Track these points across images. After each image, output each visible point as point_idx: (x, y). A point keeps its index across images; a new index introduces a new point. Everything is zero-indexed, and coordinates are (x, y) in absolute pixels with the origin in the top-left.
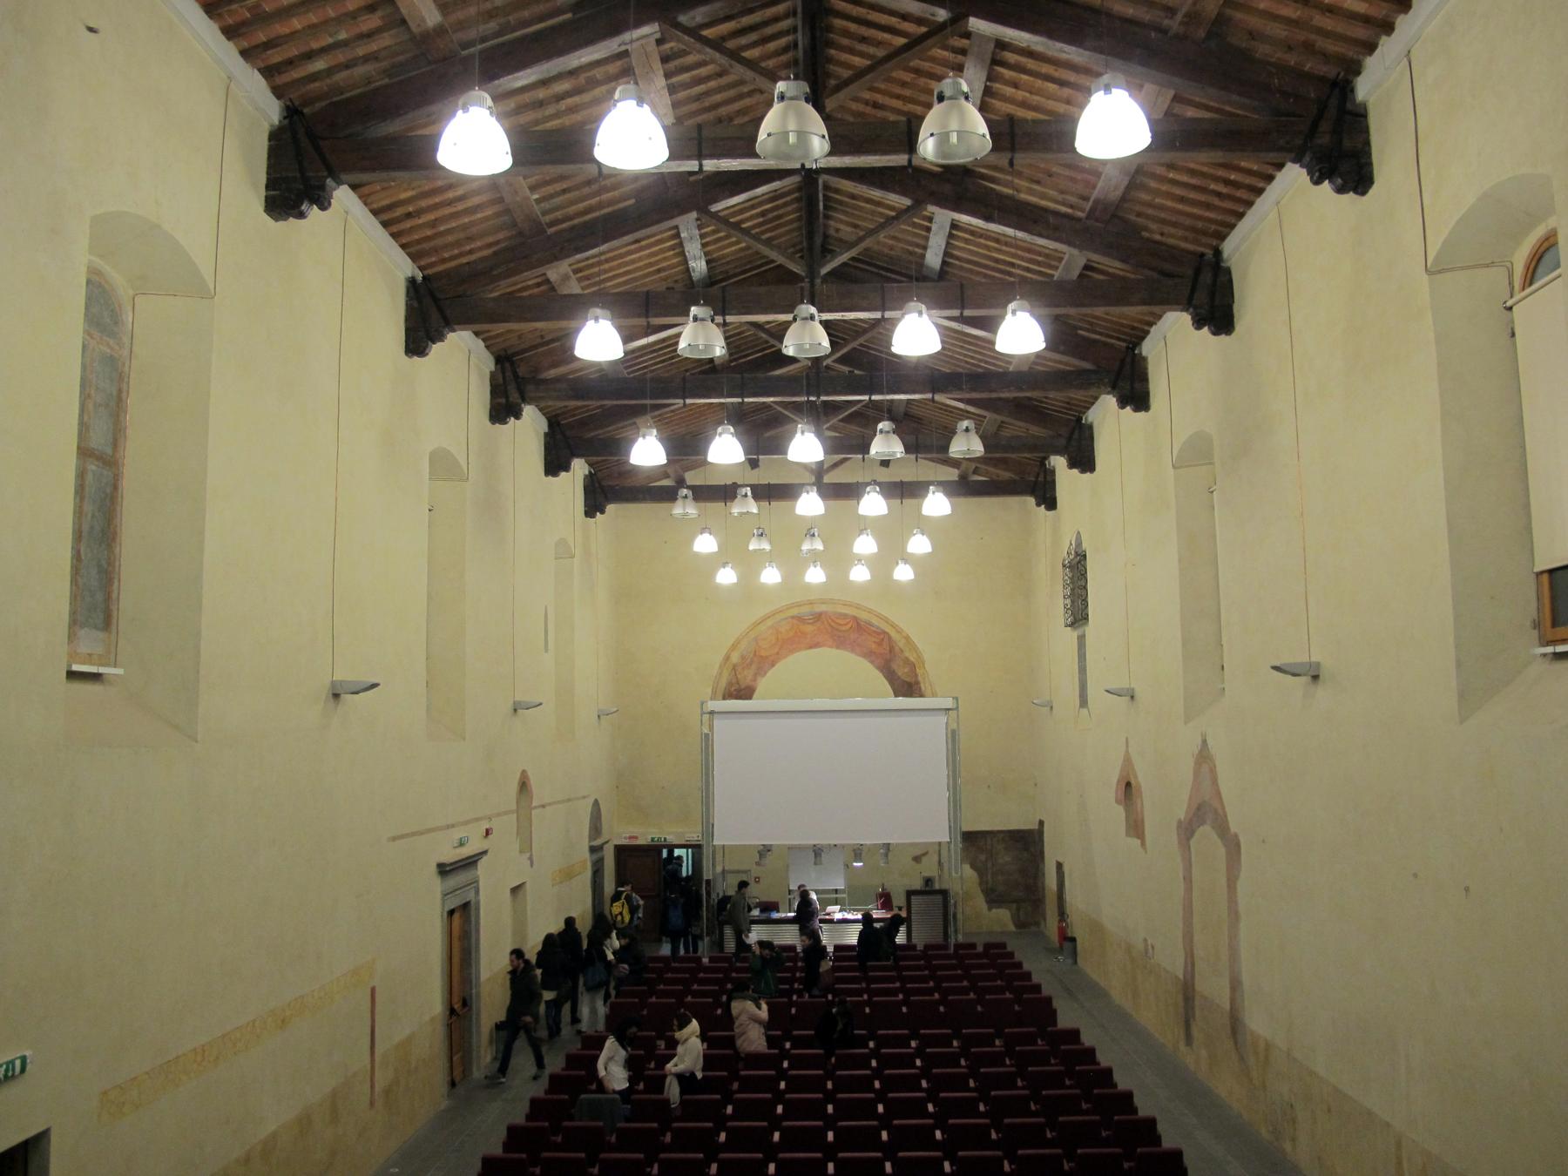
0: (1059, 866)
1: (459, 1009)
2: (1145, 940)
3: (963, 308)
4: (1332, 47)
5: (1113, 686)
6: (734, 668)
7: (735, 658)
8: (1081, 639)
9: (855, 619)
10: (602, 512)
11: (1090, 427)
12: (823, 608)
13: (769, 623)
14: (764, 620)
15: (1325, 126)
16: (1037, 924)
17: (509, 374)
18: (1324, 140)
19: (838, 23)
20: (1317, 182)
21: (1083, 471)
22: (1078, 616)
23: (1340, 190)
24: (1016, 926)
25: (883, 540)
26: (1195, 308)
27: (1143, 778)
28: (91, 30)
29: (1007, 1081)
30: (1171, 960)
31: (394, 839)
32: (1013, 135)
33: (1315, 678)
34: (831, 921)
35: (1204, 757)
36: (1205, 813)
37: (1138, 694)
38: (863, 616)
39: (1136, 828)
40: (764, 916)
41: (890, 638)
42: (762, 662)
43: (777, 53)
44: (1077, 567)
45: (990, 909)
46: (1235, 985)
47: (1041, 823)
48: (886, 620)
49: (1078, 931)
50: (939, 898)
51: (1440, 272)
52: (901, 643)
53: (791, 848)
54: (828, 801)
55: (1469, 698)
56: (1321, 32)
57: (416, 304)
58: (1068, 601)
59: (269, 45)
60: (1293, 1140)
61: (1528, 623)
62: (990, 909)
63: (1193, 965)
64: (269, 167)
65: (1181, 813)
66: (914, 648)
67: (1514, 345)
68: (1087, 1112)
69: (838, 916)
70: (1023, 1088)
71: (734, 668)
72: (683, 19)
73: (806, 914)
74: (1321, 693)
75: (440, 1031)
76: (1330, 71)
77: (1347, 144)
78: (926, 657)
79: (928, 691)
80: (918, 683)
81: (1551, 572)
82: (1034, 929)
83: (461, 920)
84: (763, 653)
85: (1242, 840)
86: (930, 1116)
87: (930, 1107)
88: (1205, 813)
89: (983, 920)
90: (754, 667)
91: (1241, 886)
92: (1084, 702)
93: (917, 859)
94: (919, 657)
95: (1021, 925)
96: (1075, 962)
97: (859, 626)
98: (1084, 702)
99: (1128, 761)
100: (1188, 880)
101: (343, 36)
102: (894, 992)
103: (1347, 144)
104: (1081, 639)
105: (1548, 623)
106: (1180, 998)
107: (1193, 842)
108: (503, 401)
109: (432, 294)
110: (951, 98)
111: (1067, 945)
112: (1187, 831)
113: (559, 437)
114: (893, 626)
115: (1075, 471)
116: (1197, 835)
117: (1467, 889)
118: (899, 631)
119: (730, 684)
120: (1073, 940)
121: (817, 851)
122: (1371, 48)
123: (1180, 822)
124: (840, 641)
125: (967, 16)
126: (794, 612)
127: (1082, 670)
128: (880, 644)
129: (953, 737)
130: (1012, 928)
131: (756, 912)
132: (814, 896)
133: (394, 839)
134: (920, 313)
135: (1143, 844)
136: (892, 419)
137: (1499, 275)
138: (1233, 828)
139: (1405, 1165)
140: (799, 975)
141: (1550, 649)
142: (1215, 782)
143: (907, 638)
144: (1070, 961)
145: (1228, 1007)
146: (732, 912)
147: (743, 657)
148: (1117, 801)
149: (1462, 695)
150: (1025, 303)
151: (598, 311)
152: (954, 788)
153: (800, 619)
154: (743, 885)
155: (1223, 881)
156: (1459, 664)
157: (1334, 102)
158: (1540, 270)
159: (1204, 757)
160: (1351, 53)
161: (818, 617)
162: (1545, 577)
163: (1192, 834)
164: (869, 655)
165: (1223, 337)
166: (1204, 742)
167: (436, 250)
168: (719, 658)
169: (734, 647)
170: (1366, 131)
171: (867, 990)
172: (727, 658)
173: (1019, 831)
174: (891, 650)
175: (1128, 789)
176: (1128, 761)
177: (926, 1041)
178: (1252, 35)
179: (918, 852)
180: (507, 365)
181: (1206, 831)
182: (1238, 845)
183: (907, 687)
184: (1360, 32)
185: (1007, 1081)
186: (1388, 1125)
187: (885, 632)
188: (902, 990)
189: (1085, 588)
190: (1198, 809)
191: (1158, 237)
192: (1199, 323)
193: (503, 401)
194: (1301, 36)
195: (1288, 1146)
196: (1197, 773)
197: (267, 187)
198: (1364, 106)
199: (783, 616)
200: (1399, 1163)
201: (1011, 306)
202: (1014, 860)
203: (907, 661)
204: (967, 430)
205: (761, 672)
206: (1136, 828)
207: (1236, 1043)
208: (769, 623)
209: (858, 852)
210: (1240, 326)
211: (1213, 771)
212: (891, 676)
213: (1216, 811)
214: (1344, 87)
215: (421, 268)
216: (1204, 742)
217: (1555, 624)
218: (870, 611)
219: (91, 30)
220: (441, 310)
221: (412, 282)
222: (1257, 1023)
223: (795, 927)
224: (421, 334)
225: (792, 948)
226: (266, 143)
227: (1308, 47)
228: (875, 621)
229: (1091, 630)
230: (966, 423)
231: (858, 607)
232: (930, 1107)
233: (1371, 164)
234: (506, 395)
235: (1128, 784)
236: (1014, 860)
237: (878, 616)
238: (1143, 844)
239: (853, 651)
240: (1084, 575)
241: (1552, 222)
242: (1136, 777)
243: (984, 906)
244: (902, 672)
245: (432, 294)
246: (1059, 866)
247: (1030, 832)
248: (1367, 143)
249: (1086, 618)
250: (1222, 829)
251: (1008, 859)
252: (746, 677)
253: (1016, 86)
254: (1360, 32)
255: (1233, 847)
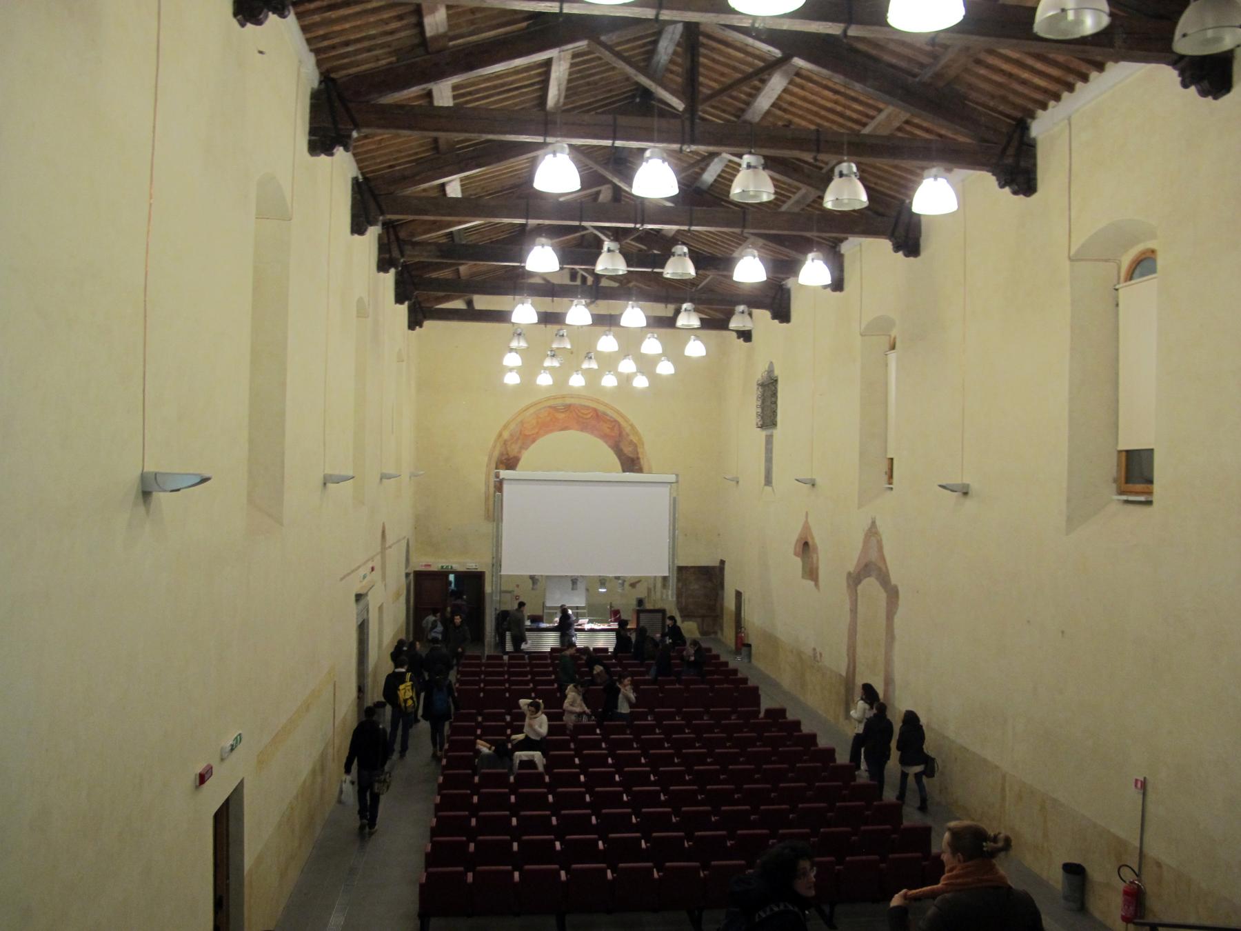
0: (739, 595)
3: (744, 227)
6: (505, 443)
7: (506, 435)
9: (595, 410)
11: (788, 291)
13: (532, 410)
14: (527, 409)
15: (1011, 151)
16: (716, 633)
17: (393, 237)
18: (1009, 161)
19: (702, 50)
21: (782, 322)
22: (768, 418)
23: (1015, 193)
25: (633, 355)
27: (819, 539)
28: (261, 52)
30: (837, 662)
31: (342, 579)
32: (818, 140)
33: (966, 494)
34: (583, 630)
35: (872, 532)
36: (870, 568)
37: (819, 481)
38: (601, 408)
39: (811, 573)
40: (535, 626)
41: (620, 425)
42: (526, 439)
44: (769, 388)
47: (722, 562)
49: (752, 640)
50: (659, 615)
52: (628, 429)
53: (547, 577)
54: (581, 544)
56: (1015, 92)
63: (854, 667)
65: (851, 567)
69: (587, 627)
70: (668, 748)
71: (505, 443)
73: (565, 626)
74: (969, 503)
75: (355, 703)
76: (1019, 115)
77: (1022, 164)
79: (645, 467)
81: (1127, 451)
84: (527, 433)
85: (900, 589)
88: (870, 568)
91: (898, 620)
92: (768, 481)
93: (633, 585)
97: (598, 416)
98: (768, 481)
100: (854, 611)
102: (527, 683)
105: (1123, 479)
106: (843, 691)
107: (860, 587)
108: (387, 256)
109: (371, 191)
111: (744, 650)
112: (855, 580)
118: (627, 421)
119: (502, 454)
120: (749, 646)
121: (574, 581)
122: (1044, 107)
124: (584, 426)
126: (551, 403)
127: (769, 460)
128: (612, 429)
129: (674, 503)
131: (528, 623)
132: (570, 612)
133: (342, 579)
135: (817, 585)
138: (894, 580)
141: (1125, 498)
142: (880, 548)
143: (632, 426)
144: (746, 660)
146: (513, 623)
148: (796, 554)
149: (1069, 519)
151: (543, 240)
152: (673, 538)
153: (555, 408)
154: (522, 604)
156: (1069, 501)
158: (1137, 272)
159: (872, 532)
160: (1030, 106)
161: (568, 408)
163: (859, 582)
164: (604, 437)
166: (874, 523)
167: (373, 158)
168: (494, 436)
169: (505, 427)
170: (1034, 157)
171: (508, 681)
172: (500, 435)
174: (620, 434)
175: (805, 547)
177: (659, 718)
183: (631, 463)
187: (616, 421)
188: (532, 681)
189: (775, 403)
190: (866, 565)
192: (897, 248)
193: (387, 256)
198: (1034, 140)
201: (810, 256)
203: (631, 442)
205: (525, 446)
206: (811, 573)
208: (532, 410)
209: (603, 581)
210: (925, 254)
211: (880, 543)
213: (880, 569)
216: (874, 523)
217: (1127, 481)
218: (606, 405)
219: (261, 52)
221: (355, 180)
223: (557, 634)
225: (606, 650)
227: (1004, 99)
228: (609, 412)
229: (777, 433)
231: (597, 401)
234: (390, 251)
235: (806, 544)
237: (612, 408)
238: (817, 585)
239: (592, 433)
244: (627, 450)
246: (739, 595)
247: (713, 568)
248: (1035, 165)
250: (884, 580)
251: (696, 587)
252: (513, 450)
253: (802, 88)
255: (893, 594)
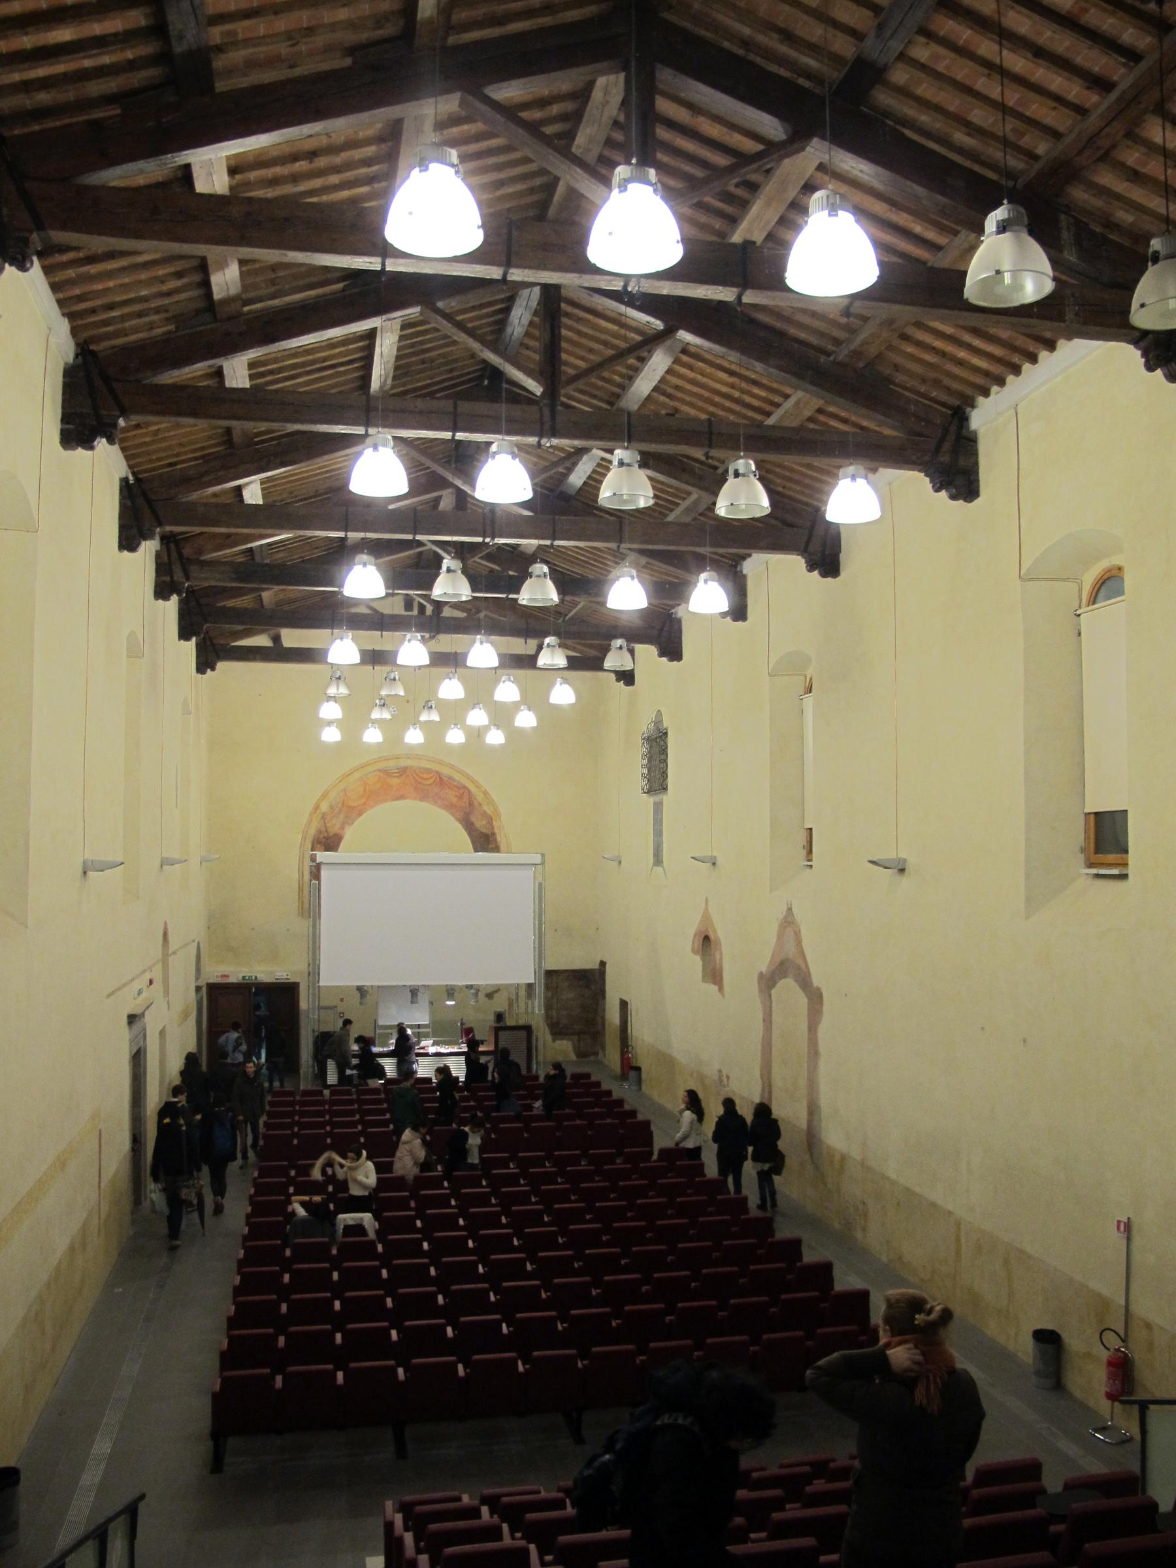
0: (624, 1004)
1: (137, 1140)
2: (720, 1071)
4: (955, 386)
5: (697, 855)
6: (324, 816)
7: (324, 807)
8: (658, 808)
10: (213, 669)
12: (408, 763)
13: (357, 775)
15: (946, 446)
16: (596, 1054)
17: (174, 555)
18: (945, 458)
19: (564, 320)
20: (937, 490)
21: (671, 660)
22: (657, 781)
23: (953, 497)
24: (578, 1057)
26: (810, 554)
27: (722, 933)
29: (523, 1198)
31: (109, 996)
33: (902, 870)
34: (427, 1055)
35: (788, 921)
36: (787, 968)
38: (446, 771)
39: (714, 975)
41: (469, 791)
42: (351, 811)
43: (488, 315)
45: (554, 1041)
46: (813, 1110)
48: (468, 777)
49: (644, 1063)
50: (523, 1034)
51: (1030, 580)
52: (480, 797)
54: (418, 946)
55: (1033, 902)
57: (129, 503)
58: (645, 771)
59: (80, 298)
60: (864, 1230)
61: (1078, 849)
62: (554, 1041)
64: (64, 401)
65: (763, 966)
66: (491, 802)
67: (1080, 642)
68: (632, 1219)
70: (536, 1203)
71: (324, 816)
72: (440, 304)
74: (905, 881)
78: (502, 810)
79: (503, 846)
80: (494, 834)
81: (1096, 814)
82: (592, 1058)
83: (138, 1059)
84: (351, 804)
85: (824, 991)
86: (418, 1231)
87: (419, 1223)
88: (787, 968)
89: (555, 1051)
90: (341, 816)
92: (658, 860)
93: (490, 996)
94: (496, 810)
95: (581, 1054)
96: (640, 1089)
97: (442, 781)
98: (658, 860)
99: (706, 917)
100: (768, 1021)
101: (143, 293)
103: (962, 462)
104: (658, 808)
107: (773, 992)
108: (168, 579)
109: (144, 494)
110: (744, 475)
111: (632, 1074)
112: (768, 982)
113: (193, 603)
114: (473, 781)
115: (665, 659)
116: (778, 985)
117: (1025, 1041)
119: (320, 832)
121: (414, 992)
122: (986, 393)
123: (761, 975)
124: (423, 794)
125: (677, 329)
126: (382, 765)
128: (460, 797)
130: (573, 1057)
132: (409, 1032)
134: (633, 578)
135: (721, 989)
136: (557, 634)
137: (1073, 587)
139: (963, 1240)
140: (437, 1104)
141: (1094, 871)
143: (486, 793)
144: (634, 1088)
145: (804, 1126)
147: (332, 807)
148: (694, 951)
149: (1028, 900)
150: (714, 574)
151: (365, 557)
152: (540, 936)
153: (386, 772)
155: (804, 1026)
157: (953, 428)
159: (788, 921)
160: (969, 391)
161: (403, 771)
162: (1092, 817)
164: (450, 807)
165: (829, 579)
168: (310, 808)
169: (324, 796)
170: (975, 454)
172: (317, 807)
173: (585, 971)
174: (471, 804)
175: (706, 942)
176: (706, 917)
178: (897, 367)
179: (490, 990)
180: (172, 546)
181: (788, 988)
182: (821, 996)
183: (485, 841)
184: (979, 380)
185: (523, 1198)
186: (950, 1213)
187: (464, 787)
189: (665, 761)
191: (780, 489)
193: (168, 579)
194: (933, 375)
195: (859, 1235)
196: (781, 935)
197: (63, 421)
198: (975, 433)
199: (370, 769)
200: (958, 1240)
201: (703, 576)
202: (579, 995)
203: (485, 814)
204: (621, 648)
205: (348, 821)
206: (714, 975)
207: (811, 1155)
208: (357, 775)
209: (450, 992)
210: (843, 573)
212: (469, 827)
213: (799, 968)
214: (960, 416)
215: (133, 474)
216: (790, 909)
217: (1098, 849)
218: (452, 767)
220: (154, 513)
221: (124, 482)
222: (834, 1138)
224: (134, 531)
226: (60, 379)
227: (937, 383)
228: (457, 776)
229: (667, 799)
230: (619, 642)
231: (441, 763)
232: (419, 1223)
233: (978, 481)
234: (170, 573)
235: (707, 938)
236: (579, 995)
237: (459, 771)
238: (721, 989)
239: (435, 803)
240: (664, 751)
241: (1116, 560)
242: (715, 931)
243: (549, 1037)
244: (480, 824)
245: (144, 494)
246: (624, 1004)
247: (591, 971)
248: (976, 464)
249: (665, 789)
250: (805, 982)
251: (571, 995)
252: (334, 826)
254: (979, 380)
255: (815, 998)
